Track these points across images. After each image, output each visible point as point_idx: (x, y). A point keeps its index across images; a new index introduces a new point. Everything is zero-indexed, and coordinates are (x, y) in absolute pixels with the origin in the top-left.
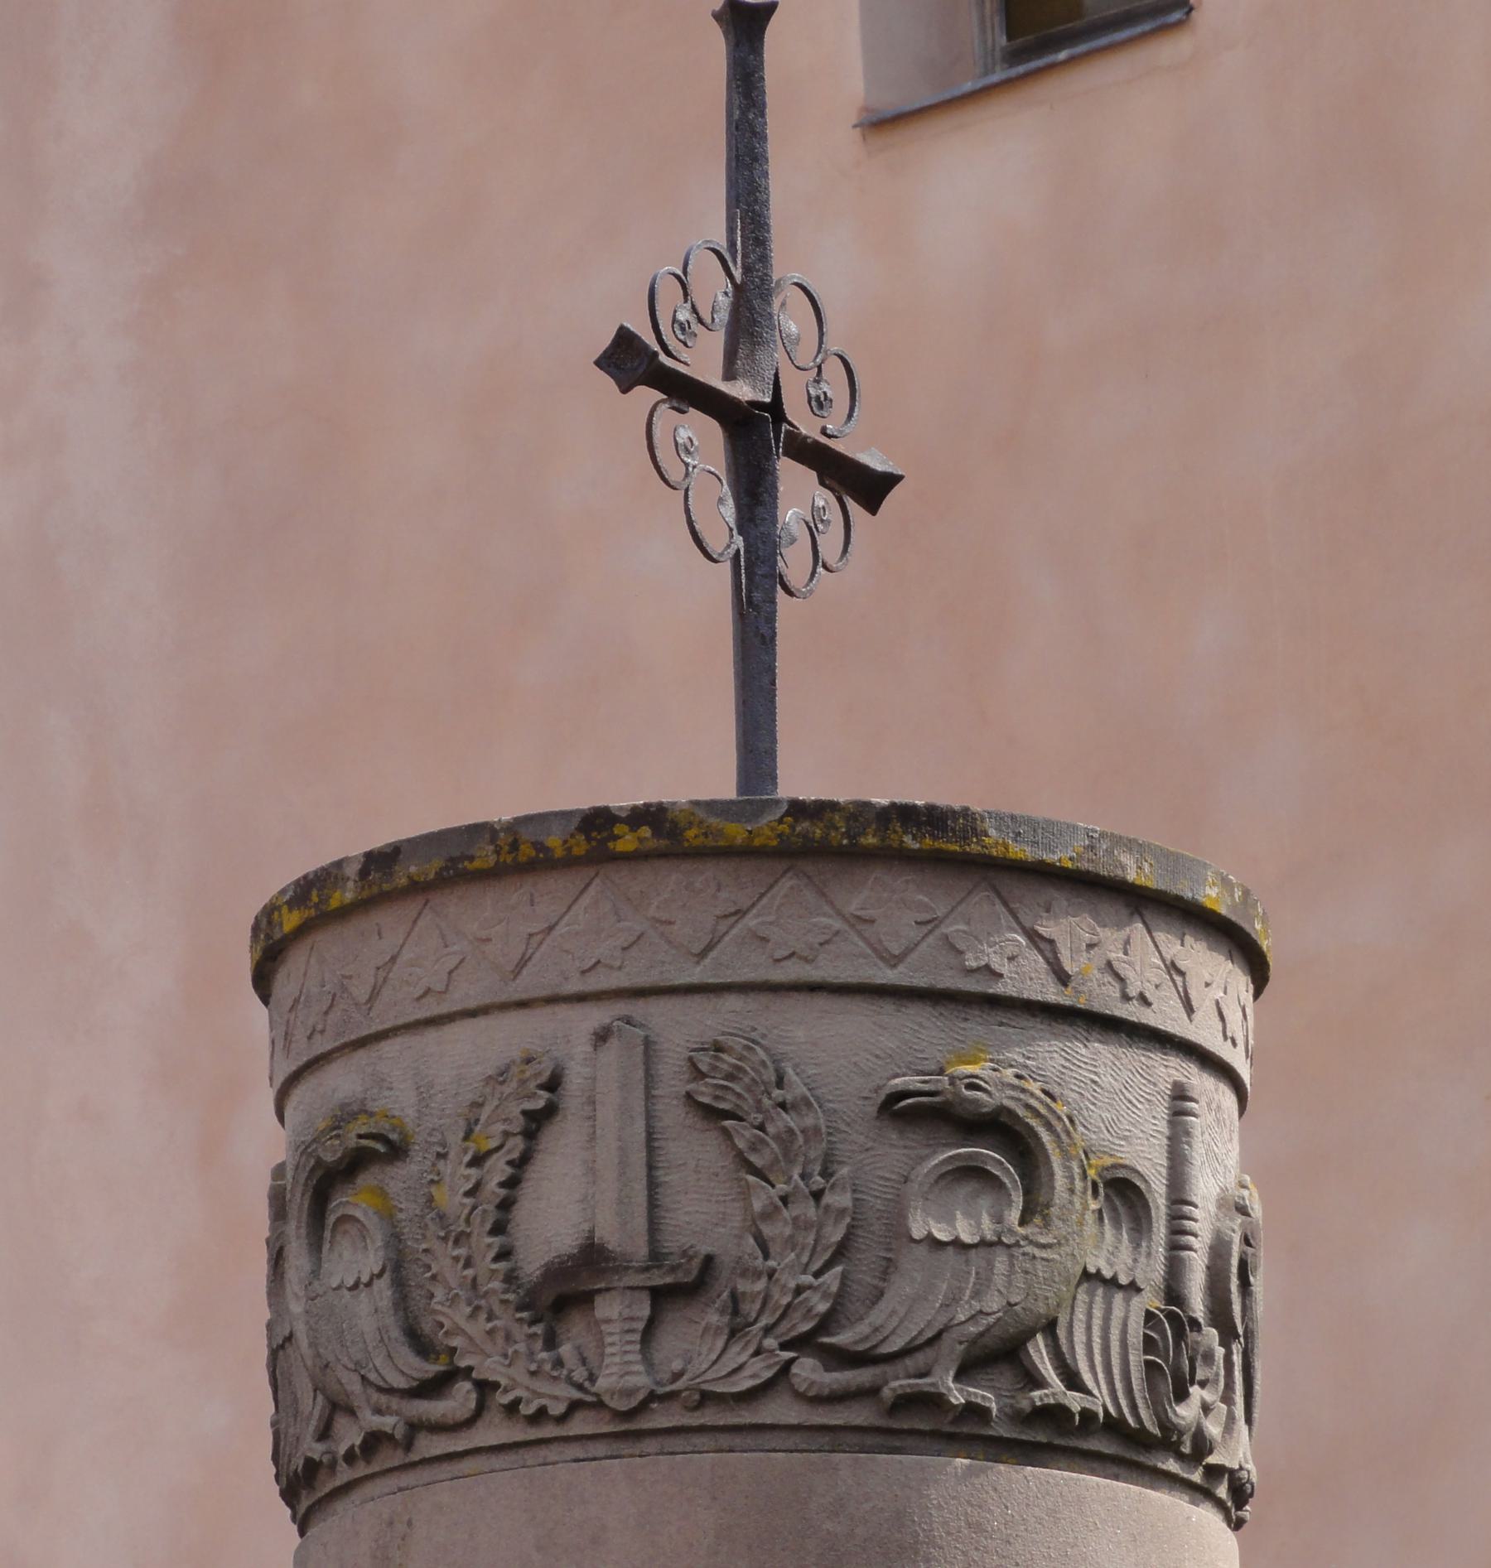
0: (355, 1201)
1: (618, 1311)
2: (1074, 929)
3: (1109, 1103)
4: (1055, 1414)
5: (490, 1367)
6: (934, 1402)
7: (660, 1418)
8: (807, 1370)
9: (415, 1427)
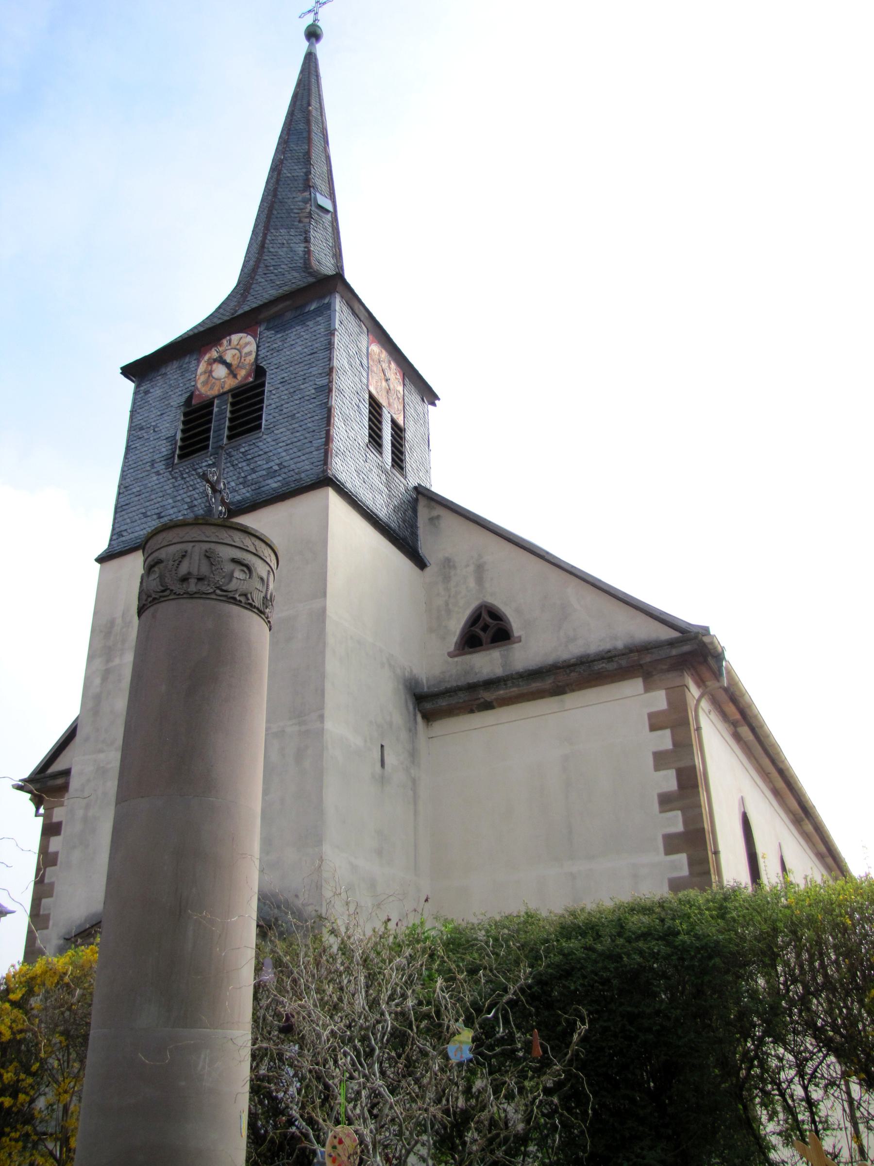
0: (156, 569)
1: (193, 581)
2: (258, 543)
3: (261, 569)
4: (251, 605)
5: (171, 588)
6: (235, 599)
7: (196, 596)
8: (218, 592)
9: (161, 597)
